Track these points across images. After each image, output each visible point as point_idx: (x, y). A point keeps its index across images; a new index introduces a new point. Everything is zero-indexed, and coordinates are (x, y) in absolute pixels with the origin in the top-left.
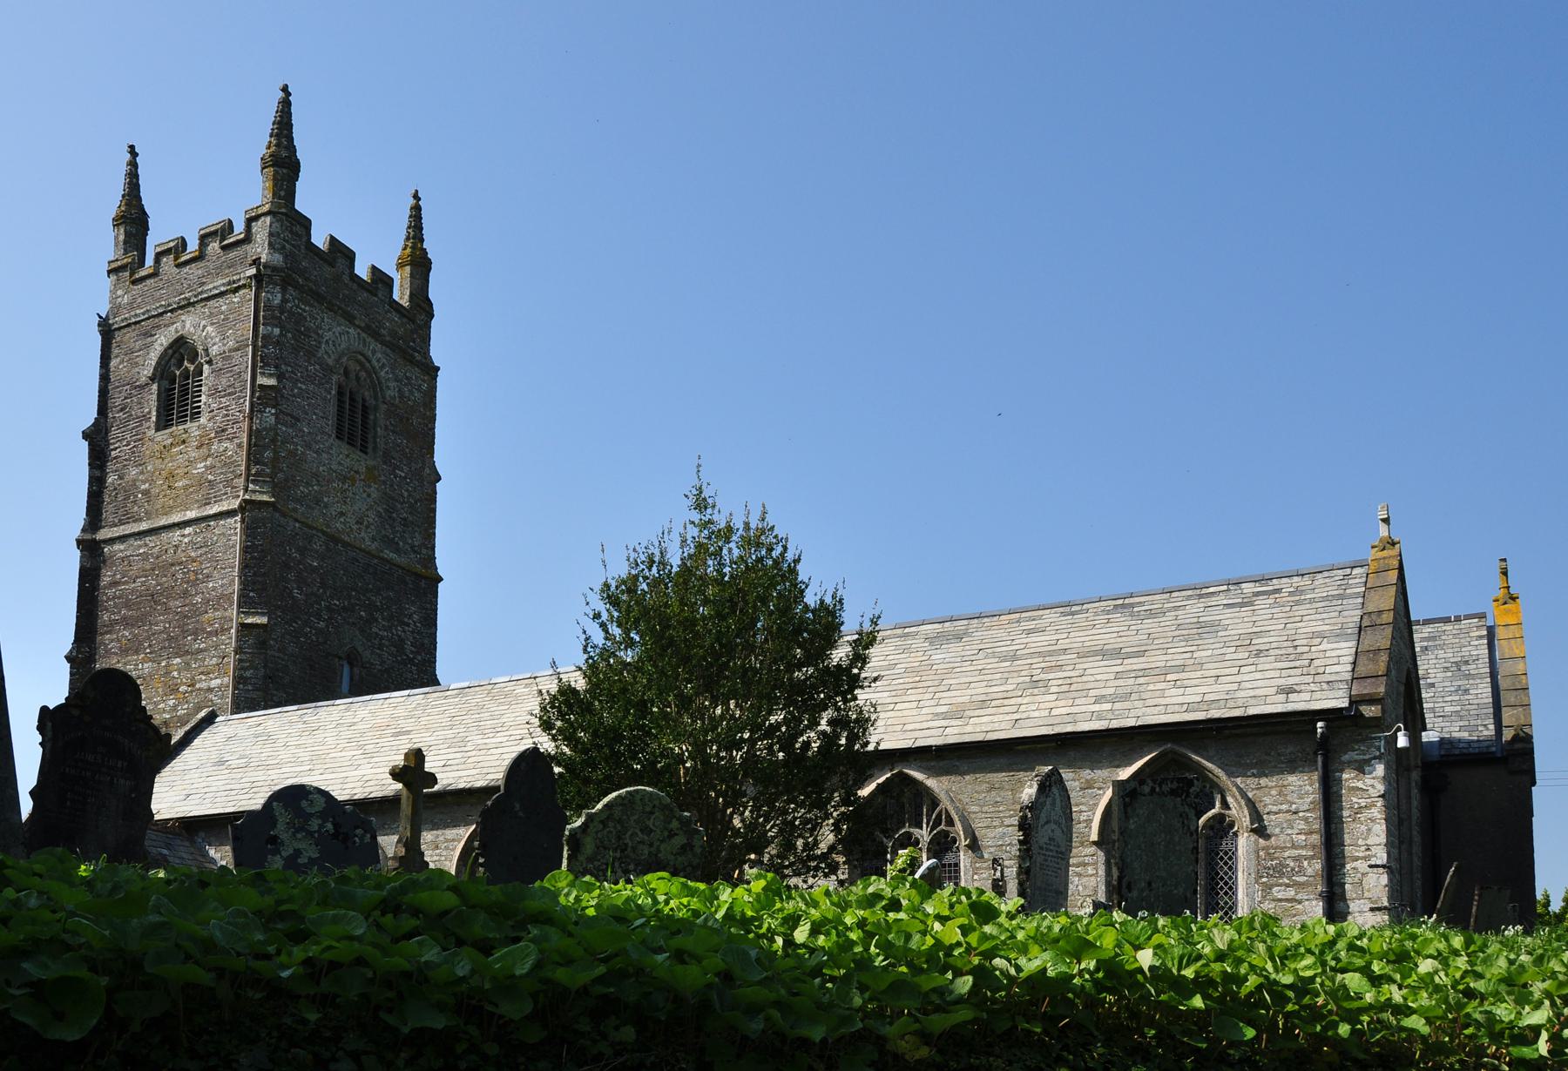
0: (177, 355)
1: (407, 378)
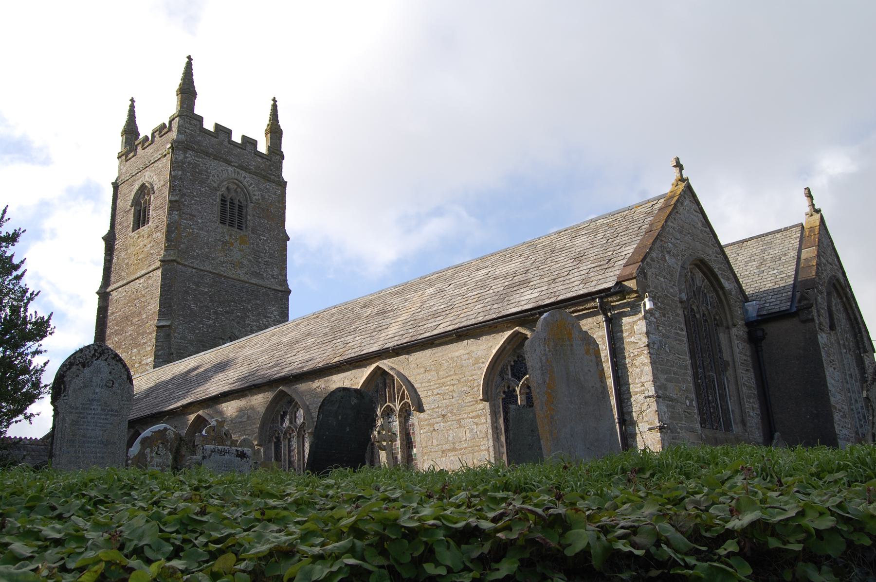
1: (267, 189)
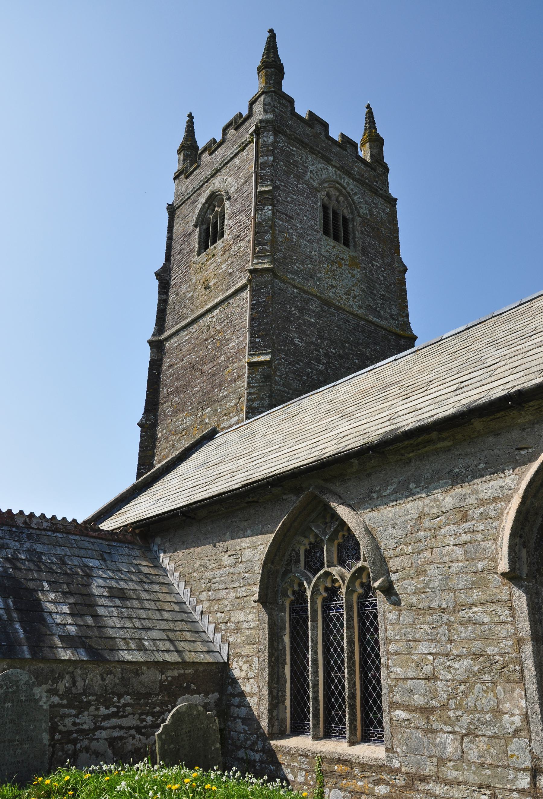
0: (210, 207)
1: (374, 203)
